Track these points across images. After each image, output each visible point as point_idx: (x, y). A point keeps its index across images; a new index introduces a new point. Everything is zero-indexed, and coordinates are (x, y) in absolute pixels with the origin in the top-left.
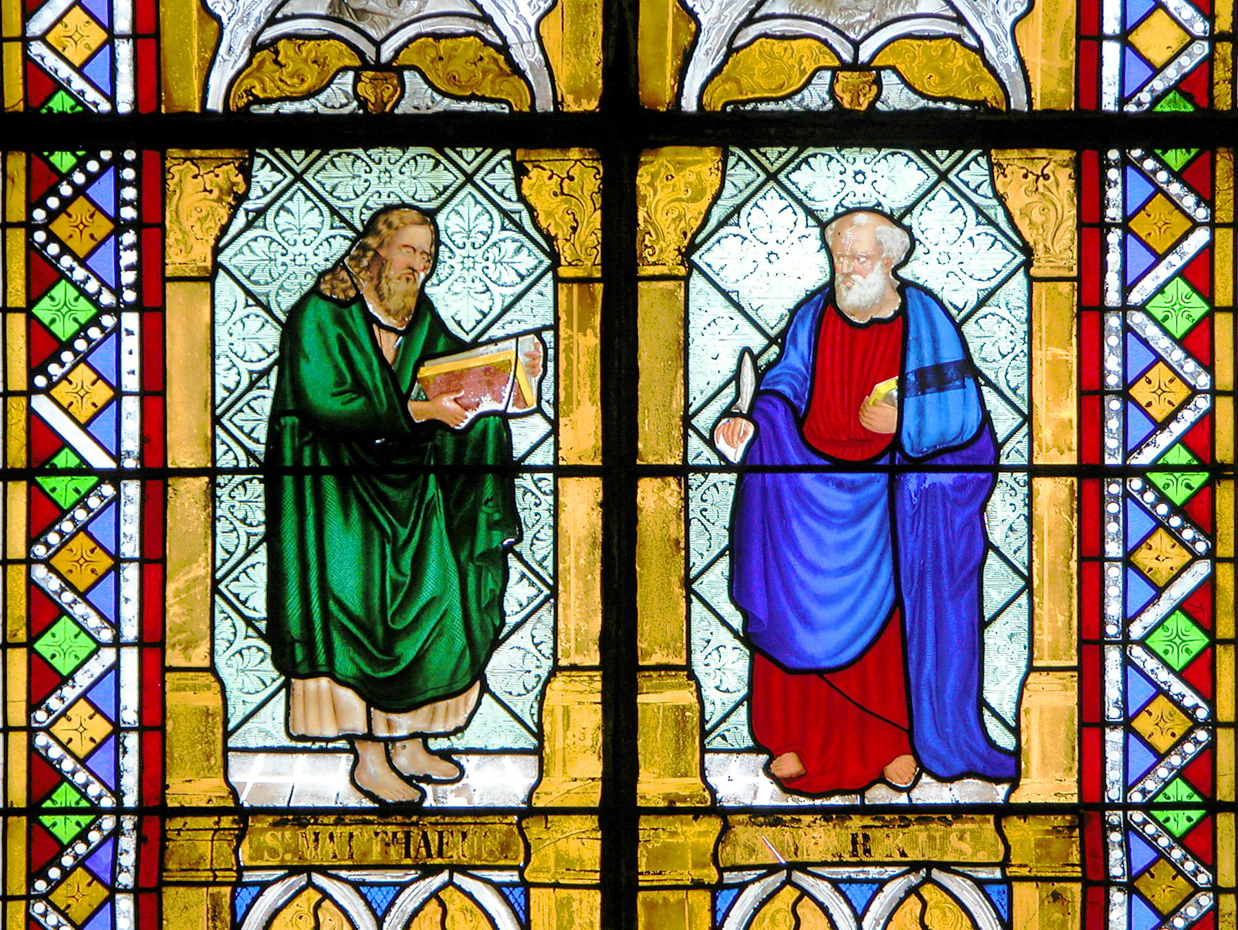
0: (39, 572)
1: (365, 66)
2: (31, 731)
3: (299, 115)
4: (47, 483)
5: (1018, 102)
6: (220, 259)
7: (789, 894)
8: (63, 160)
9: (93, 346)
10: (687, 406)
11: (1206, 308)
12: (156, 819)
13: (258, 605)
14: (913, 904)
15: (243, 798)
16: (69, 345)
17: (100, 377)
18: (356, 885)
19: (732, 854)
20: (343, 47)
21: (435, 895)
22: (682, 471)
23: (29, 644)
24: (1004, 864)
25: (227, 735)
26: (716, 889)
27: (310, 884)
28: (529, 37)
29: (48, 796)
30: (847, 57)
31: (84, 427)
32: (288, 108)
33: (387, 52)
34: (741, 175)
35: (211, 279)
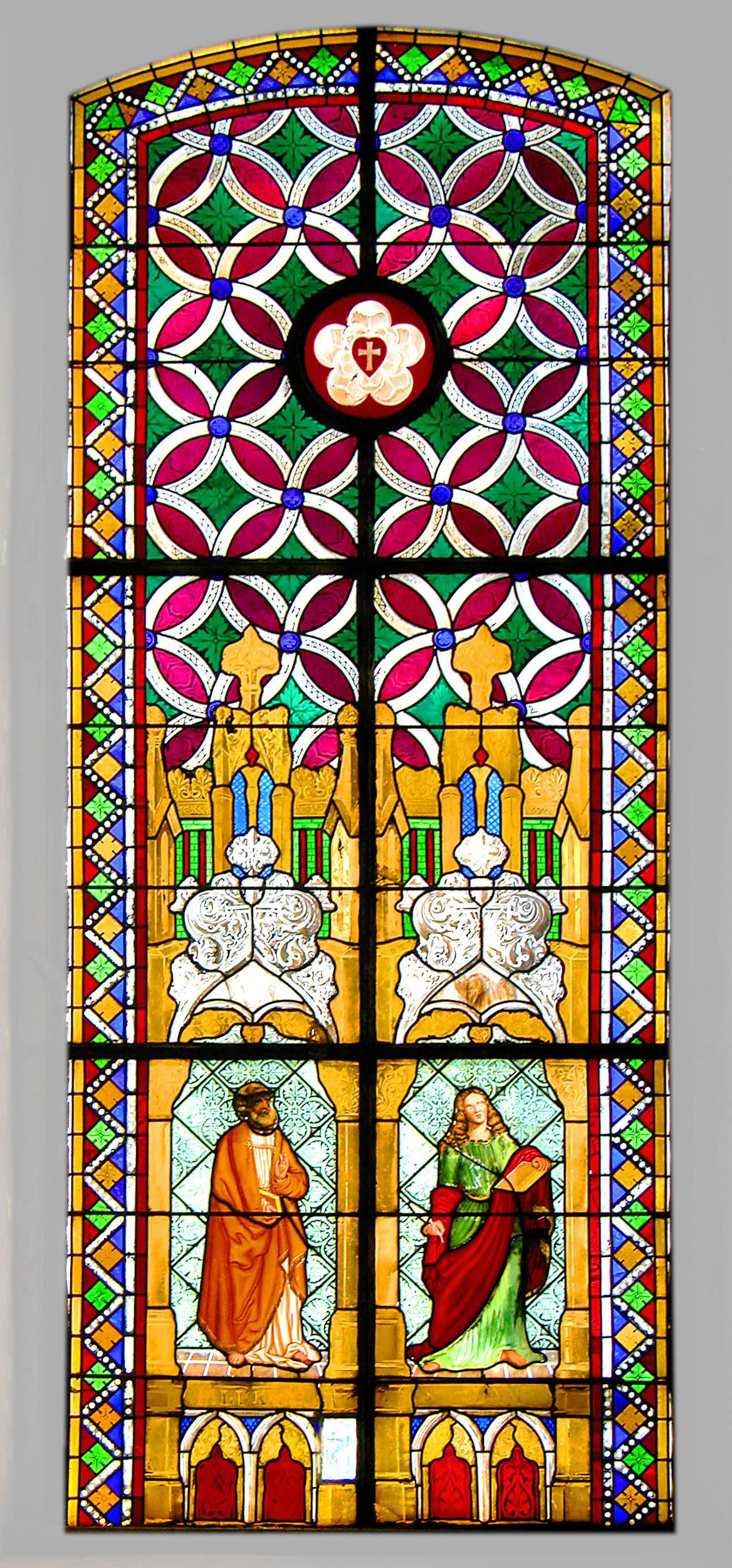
0: (88, 1179)
1: (247, 1023)
2: (80, 1499)
3: (212, 1044)
4: (92, 1218)
5: (561, 1039)
6: (175, 1112)
7: (449, 1421)
8: (101, 1063)
9: (113, 904)
10: (399, 1183)
11: (650, 1135)
12: (142, 1381)
13: (195, 1278)
14: (510, 1428)
15: (184, 1371)
16: (102, 824)
17: (116, 839)
18: (240, 1418)
19: (421, 1400)
20: (235, 1014)
21: (278, 1423)
22: (396, 1213)
23: (82, 1296)
24: (553, 1409)
25: (177, 1339)
26: (412, 1416)
27: (218, 1417)
28: (325, 1010)
29: (92, 880)
30: (477, 1021)
31: (108, 944)
32: (209, 1041)
33: (257, 1016)
34: (426, 1071)
35: (171, 1120)
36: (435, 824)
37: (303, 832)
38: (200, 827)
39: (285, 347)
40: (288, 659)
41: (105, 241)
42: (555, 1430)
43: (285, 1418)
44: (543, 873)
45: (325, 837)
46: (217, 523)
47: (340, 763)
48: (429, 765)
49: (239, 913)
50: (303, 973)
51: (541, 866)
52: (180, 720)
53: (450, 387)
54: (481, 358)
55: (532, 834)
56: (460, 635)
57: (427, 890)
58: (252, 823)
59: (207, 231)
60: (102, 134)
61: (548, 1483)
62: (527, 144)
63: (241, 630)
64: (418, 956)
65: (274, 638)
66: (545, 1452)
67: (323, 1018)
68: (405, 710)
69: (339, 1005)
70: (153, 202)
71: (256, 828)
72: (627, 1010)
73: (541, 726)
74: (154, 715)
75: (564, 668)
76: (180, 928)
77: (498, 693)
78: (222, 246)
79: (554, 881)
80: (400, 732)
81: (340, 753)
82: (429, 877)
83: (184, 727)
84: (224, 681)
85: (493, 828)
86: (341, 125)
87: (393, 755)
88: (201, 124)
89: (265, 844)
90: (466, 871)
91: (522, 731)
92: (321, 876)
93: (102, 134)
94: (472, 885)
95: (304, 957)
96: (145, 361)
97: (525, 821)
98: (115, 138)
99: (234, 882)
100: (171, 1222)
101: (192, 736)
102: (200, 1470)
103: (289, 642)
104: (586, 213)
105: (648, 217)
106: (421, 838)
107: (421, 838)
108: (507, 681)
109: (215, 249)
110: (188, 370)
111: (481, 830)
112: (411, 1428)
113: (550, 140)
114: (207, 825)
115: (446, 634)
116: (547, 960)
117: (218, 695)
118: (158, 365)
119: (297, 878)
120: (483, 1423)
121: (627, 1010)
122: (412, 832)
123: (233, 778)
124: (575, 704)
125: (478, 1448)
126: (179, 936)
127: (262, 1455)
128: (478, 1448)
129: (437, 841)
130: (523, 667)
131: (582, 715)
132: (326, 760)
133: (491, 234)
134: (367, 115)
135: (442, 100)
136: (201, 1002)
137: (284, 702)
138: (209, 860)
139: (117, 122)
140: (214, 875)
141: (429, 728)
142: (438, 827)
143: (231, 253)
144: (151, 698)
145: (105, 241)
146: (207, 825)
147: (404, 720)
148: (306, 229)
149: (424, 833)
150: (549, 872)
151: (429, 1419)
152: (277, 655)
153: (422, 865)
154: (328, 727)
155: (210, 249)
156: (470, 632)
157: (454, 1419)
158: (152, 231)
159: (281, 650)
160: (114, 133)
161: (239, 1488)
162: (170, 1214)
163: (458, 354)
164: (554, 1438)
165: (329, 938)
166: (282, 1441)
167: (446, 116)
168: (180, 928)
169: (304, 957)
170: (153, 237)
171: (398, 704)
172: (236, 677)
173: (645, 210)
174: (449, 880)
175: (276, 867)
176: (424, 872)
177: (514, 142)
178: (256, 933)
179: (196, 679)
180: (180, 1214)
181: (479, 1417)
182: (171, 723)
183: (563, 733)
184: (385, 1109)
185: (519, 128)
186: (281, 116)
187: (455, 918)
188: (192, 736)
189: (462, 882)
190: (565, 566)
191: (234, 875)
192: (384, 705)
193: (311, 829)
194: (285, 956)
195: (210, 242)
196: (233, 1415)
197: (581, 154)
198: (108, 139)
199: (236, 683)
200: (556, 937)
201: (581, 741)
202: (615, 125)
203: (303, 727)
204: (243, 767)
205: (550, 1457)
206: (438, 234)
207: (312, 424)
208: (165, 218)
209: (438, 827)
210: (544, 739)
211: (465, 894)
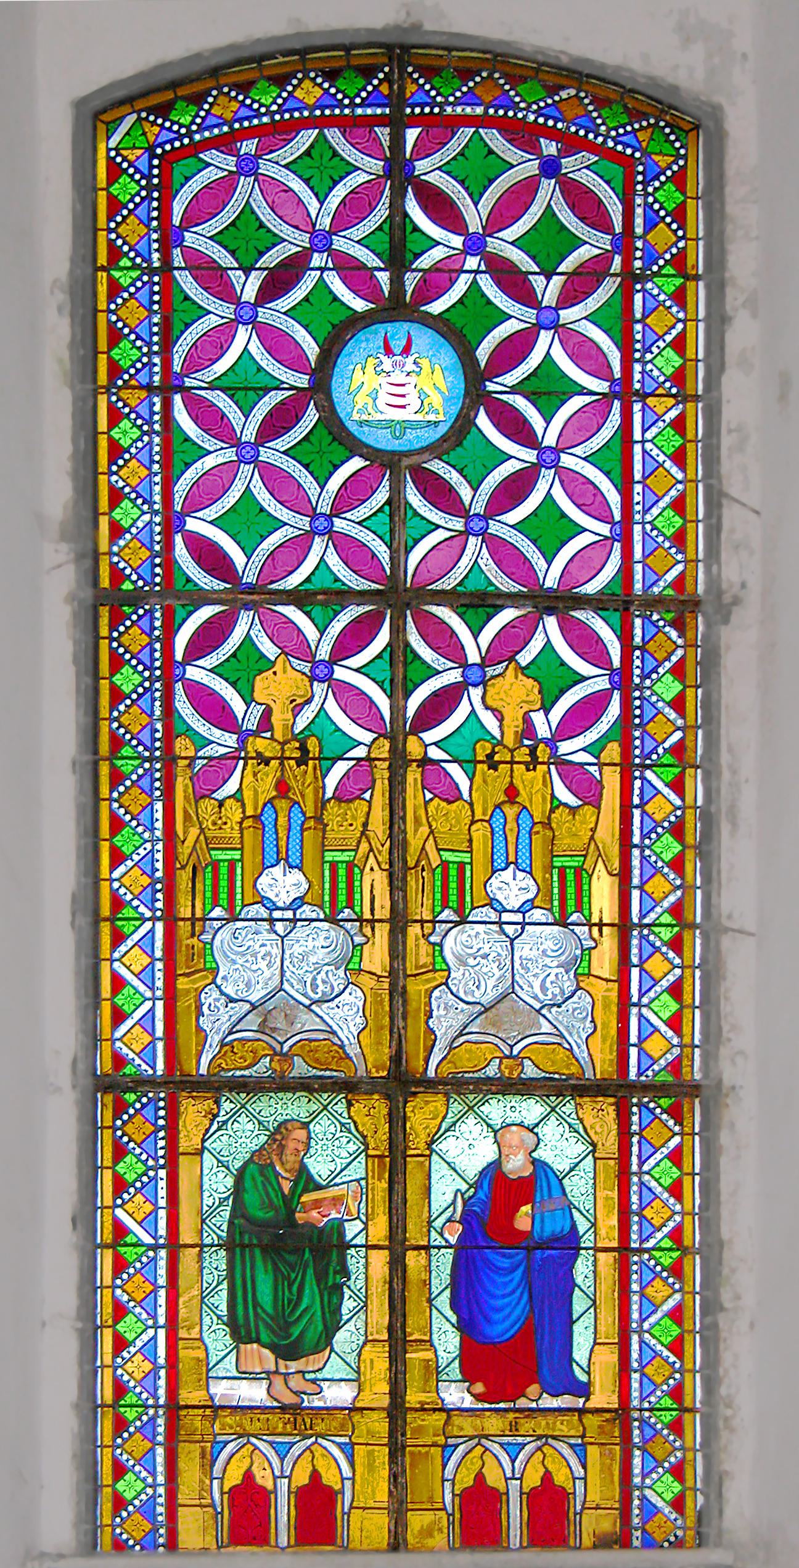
1: (276, 1054)
5: (589, 1074)
7: (480, 1449)
26: (444, 1447)
27: (249, 1442)
33: (286, 1048)
36: (465, 858)
37: (334, 866)
38: (229, 857)
39: (313, 373)
40: (319, 688)
41: (129, 264)
42: (353, 1456)
43: (547, 1443)
44: (344, 904)
45: (356, 870)
46: (547, 555)
47: (372, 795)
48: (462, 799)
49: (497, 944)
50: (332, 1004)
51: (342, 898)
52: (207, 752)
53: (483, 421)
54: (513, 390)
55: (562, 871)
56: (490, 671)
57: (457, 924)
58: (512, 859)
59: (233, 253)
60: (125, 153)
61: (346, 1510)
62: (564, 171)
63: (273, 659)
64: (449, 988)
65: (306, 667)
66: (574, 1479)
67: (582, 1054)
68: (435, 744)
69: (596, 1042)
70: (176, 221)
71: (516, 863)
72: (654, 1046)
73: (570, 762)
74: (182, 747)
75: (592, 708)
76: (439, 959)
77: (529, 729)
78: (247, 271)
79: (356, 913)
80: (425, 762)
81: (373, 788)
82: (460, 910)
83: (210, 759)
84: (257, 711)
85: (294, 859)
86: (371, 149)
87: (423, 788)
88: (226, 144)
89: (296, 876)
90: (527, 907)
91: (552, 767)
92: (353, 909)
93: (125, 153)
94: (503, 920)
95: (562, 992)
96: (171, 385)
97: (326, 854)
98: (138, 158)
99: (493, 916)
100: (430, 1255)
101: (222, 767)
102: (235, 1493)
103: (321, 671)
104: (625, 243)
105: (683, 253)
106: (453, 872)
107: (453, 872)
108: (538, 718)
109: (542, 277)
110: (520, 403)
111: (512, 866)
112: (443, 1457)
113: (587, 167)
114: (237, 855)
115: (475, 669)
116: (348, 991)
117: (252, 724)
118: (185, 391)
119: (327, 911)
120: (282, 1449)
121: (654, 1046)
122: (445, 865)
123: (263, 810)
124: (604, 741)
125: (277, 1473)
126: (438, 967)
127: (225, 1481)
128: (509, 1474)
129: (468, 874)
130: (553, 704)
131: (613, 751)
132: (358, 793)
133: (225, 259)
134: (398, 141)
135: (322, 123)
136: (461, 1035)
137: (315, 733)
138: (239, 890)
139: (141, 142)
140: (244, 906)
141: (460, 763)
142: (469, 860)
143: (557, 281)
144: (179, 728)
145: (129, 264)
146: (237, 855)
147: (435, 753)
148: (337, 256)
149: (456, 866)
150: (579, 909)
151: (462, 1447)
152: (308, 684)
153: (453, 899)
154: (359, 760)
155: (536, 277)
156: (499, 668)
157: (253, 1444)
158: (177, 252)
159: (313, 678)
160: (139, 152)
161: (293, 1513)
162: (427, 1248)
163: (491, 387)
164: (352, 1464)
165: (589, 975)
166: (313, 1466)
167: (482, 139)
168: (439, 959)
169: (562, 992)
170: (178, 260)
171: (429, 736)
172: (268, 706)
173: (681, 244)
174: (476, 915)
175: (306, 900)
176: (455, 906)
177: (550, 168)
178: (286, 963)
179: (374, 710)
180: (439, 1248)
181: (278, 1443)
182: (200, 754)
183: (593, 769)
184: (417, 1142)
185: (556, 154)
186: (306, 138)
187: (486, 950)
188: (222, 767)
189: (493, 916)
190: (598, 603)
191: (264, 905)
192: (415, 738)
193: (570, 867)
194: (314, 987)
195: (236, 266)
196: (333, 1442)
197: (618, 183)
198: (132, 158)
199: (267, 713)
200: (586, 971)
201: (612, 780)
202: (653, 157)
203: (335, 760)
204: (273, 798)
205: (348, 1483)
206: (472, 262)
207: (340, 452)
208: (189, 238)
209: (469, 860)
210: (571, 773)
211: (495, 927)
